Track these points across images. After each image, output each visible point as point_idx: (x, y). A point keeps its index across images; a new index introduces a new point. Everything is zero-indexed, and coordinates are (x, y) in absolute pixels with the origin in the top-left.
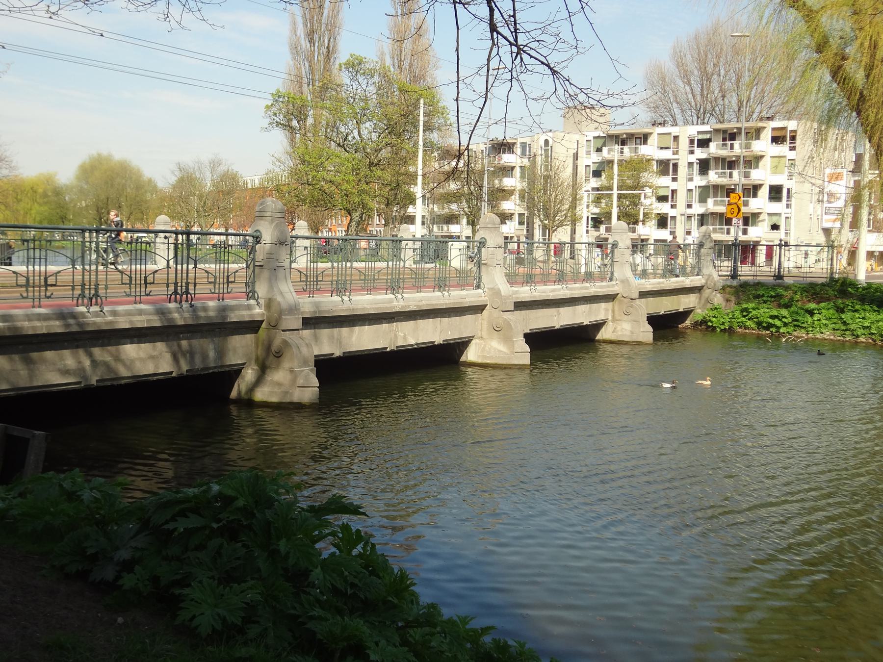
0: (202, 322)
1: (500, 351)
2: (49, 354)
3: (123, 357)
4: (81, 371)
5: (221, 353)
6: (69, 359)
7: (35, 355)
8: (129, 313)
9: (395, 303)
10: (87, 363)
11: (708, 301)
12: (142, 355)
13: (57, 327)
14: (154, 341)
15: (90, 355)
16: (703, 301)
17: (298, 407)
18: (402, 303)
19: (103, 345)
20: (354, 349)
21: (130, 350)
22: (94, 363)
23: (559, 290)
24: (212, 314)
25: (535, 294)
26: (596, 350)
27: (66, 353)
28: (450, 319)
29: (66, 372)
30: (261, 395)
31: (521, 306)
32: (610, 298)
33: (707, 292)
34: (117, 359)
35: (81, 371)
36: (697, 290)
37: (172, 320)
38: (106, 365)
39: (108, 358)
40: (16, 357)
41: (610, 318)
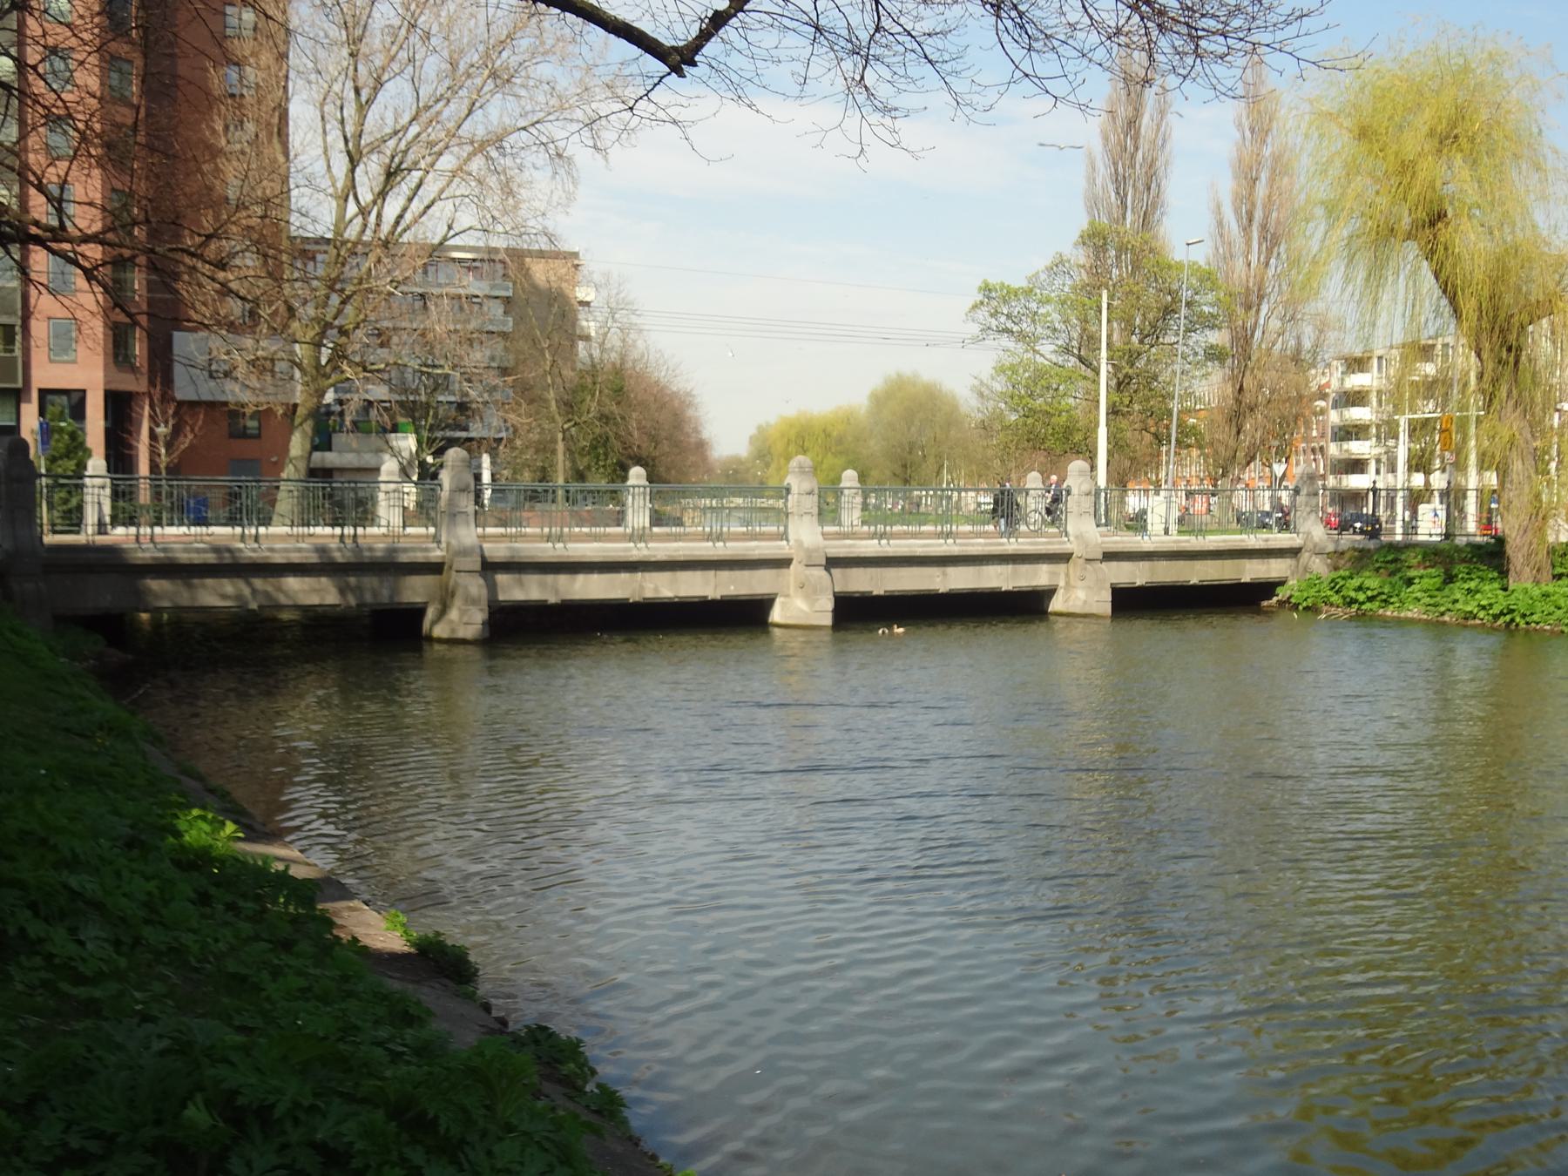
0: (366, 560)
1: (802, 611)
2: (209, 582)
3: (285, 588)
4: (239, 597)
5: (395, 591)
6: (229, 586)
7: (196, 581)
8: (286, 550)
9: (635, 552)
10: (247, 591)
11: (1306, 569)
12: (306, 587)
13: (211, 558)
14: (320, 576)
15: (249, 584)
16: (1301, 569)
17: (463, 642)
18: (645, 552)
19: (265, 577)
20: (577, 597)
21: (292, 583)
22: (254, 591)
23: (941, 545)
24: (379, 554)
25: (888, 549)
26: (1047, 620)
27: (225, 581)
28: (732, 573)
29: (224, 597)
30: (440, 631)
31: (1109, 556)
32: (1065, 558)
33: (1305, 556)
34: (280, 589)
35: (239, 597)
36: (1294, 552)
37: (333, 558)
38: (267, 594)
39: (269, 589)
40: (179, 582)
41: (1062, 583)
